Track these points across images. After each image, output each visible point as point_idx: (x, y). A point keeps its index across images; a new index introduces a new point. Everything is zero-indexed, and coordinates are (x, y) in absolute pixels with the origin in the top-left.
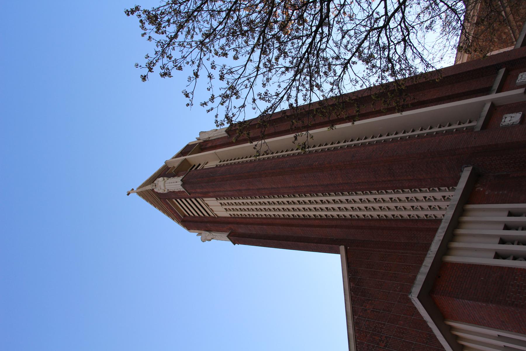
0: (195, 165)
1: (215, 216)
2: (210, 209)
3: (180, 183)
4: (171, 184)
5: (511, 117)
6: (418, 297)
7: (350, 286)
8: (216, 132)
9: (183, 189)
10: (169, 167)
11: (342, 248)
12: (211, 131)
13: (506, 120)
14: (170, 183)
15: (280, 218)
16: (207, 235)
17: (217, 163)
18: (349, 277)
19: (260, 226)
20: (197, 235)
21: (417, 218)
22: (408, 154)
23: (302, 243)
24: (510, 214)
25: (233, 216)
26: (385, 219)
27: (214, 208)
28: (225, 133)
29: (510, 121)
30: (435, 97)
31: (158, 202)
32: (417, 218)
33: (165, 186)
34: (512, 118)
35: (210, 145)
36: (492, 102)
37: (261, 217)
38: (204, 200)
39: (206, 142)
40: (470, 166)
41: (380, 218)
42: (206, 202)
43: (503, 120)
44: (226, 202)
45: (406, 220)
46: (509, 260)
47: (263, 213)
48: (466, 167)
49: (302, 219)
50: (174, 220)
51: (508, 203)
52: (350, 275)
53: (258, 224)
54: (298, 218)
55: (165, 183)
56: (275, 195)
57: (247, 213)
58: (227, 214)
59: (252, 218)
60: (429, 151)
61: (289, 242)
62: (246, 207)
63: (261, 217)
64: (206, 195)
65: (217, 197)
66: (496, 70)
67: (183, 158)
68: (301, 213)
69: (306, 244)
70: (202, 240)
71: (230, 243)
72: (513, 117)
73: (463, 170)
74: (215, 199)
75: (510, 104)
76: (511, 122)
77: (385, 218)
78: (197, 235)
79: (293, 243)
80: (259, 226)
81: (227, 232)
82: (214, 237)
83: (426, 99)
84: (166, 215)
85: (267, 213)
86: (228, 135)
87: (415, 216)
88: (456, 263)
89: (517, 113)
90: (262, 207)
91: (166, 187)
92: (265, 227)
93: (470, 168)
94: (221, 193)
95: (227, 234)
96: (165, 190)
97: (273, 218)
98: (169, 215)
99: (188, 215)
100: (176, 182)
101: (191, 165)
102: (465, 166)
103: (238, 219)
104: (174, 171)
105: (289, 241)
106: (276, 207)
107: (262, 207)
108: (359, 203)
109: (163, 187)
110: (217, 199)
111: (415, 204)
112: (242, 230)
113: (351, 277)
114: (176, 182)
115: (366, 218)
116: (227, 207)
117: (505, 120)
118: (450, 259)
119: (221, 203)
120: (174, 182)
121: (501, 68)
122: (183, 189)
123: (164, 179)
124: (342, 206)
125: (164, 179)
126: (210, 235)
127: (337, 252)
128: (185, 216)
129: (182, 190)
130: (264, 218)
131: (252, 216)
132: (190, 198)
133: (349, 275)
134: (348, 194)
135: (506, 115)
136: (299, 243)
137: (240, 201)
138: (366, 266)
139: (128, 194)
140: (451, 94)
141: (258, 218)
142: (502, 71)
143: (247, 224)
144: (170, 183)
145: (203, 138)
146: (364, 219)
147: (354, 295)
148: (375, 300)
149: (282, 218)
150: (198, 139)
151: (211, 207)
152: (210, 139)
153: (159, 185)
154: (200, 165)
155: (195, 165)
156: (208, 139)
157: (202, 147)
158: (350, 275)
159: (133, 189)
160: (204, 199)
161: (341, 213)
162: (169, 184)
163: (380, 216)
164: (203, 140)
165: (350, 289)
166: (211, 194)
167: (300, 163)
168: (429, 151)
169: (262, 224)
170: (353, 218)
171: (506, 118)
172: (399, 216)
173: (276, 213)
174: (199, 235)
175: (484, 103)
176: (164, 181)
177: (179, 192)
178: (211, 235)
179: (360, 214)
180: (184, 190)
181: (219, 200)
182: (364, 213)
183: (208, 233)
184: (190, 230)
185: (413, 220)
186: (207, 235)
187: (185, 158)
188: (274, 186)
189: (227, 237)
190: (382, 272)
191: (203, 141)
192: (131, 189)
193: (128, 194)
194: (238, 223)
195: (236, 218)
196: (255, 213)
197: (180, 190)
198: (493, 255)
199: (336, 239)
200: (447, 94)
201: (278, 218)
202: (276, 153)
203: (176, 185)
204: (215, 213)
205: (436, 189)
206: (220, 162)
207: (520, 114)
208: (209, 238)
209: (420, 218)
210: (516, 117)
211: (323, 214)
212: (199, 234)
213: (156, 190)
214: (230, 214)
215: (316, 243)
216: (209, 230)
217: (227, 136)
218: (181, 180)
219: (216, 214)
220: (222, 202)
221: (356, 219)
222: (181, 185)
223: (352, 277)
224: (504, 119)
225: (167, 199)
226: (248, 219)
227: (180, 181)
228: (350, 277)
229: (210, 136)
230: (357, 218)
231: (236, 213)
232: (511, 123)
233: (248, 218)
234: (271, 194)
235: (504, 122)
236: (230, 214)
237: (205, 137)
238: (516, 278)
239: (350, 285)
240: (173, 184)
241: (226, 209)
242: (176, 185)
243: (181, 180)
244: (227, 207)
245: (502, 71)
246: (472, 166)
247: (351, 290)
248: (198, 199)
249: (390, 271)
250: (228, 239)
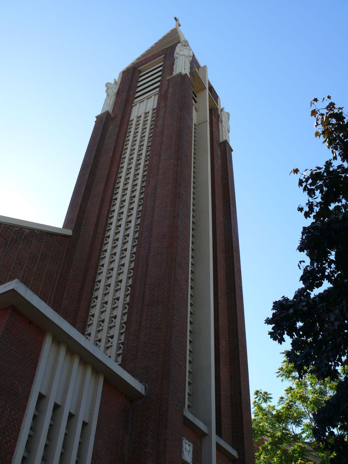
0: (196, 96)
1: (134, 103)
2: (144, 100)
3: (183, 72)
4: (184, 62)
5: (189, 452)
6: (13, 290)
7: (26, 229)
8: (226, 131)
9: (175, 74)
10: (199, 69)
11: (69, 232)
12: (229, 126)
13: (187, 446)
14: (185, 61)
15: (117, 173)
16: (113, 90)
17: (195, 121)
18: (36, 230)
19: (112, 150)
20: (115, 80)
21: (88, 323)
22: (173, 326)
23: (83, 190)
24: (85, 424)
25: (130, 123)
26: (94, 287)
27: (143, 104)
28: (224, 140)
29: (186, 449)
30: (221, 375)
31: (162, 46)
32: (88, 323)
33: (183, 55)
34: (187, 452)
35: (214, 120)
36: (207, 434)
37: (123, 153)
38: (155, 95)
39: (218, 117)
40: (145, 392)
41: (96, 282)
42: (153, 97)
43: (187, 442)
44: (149, 118)
45: (88, 311)
46: (35, 410)
47: (127, 155)
48: (146, 388)
49: (112, 197)
50: (137, 59)
51: (97, 425)
52: (37, 232)
53: (115, 148)
54: (114, 192)
55: (186, 56)
56: (147, 172)
57: (131, 138)
58: (134, 116)
59: (124, 142)
60: (172, 351)
61: (88, 176)
62: (138, 138)
63: (123, 153)
64: (162, 98)
65: (157, 111)
66: (237, 448)
67: (207, 87)
68: (119, 196)
69: (83, 194)
70: (106, 84)
71: (99, 112)
72: (188, 454)
73: (143, 384)
74: (155, 107)
75: (201, 454)
76: (185, 450)
77: (95, 288)
78: (115, 80)
79: (86, 180)
80: (113, 148)
81: (112, 112)
82: (110, 97)
83: (221, 365)
84: (162, 38)
85: (126, 160)
86: (221, 143)
87: (91, 322)
88: (42, 347)
89: (192, 458)
90: (135, 156)
91: (181, 57)
92: (111, 154)
93: (143, 392)
94: (161, 114)
95: (111, 112)
96: (178, 54)
97: (119, 165)
98: (143, 56)
99: (140, 75)
100: (185, 69)
101: (197, 93)
102: (147, 388)
103: (126, 127)
104: (196, 71)
105: (89, 176)
106: (132, 171)
107: (135, 156)
108: (119, 262)
109: (181, 53)
110: (154, 110)
111: (106, 325)
112: (112, 129)
113: (36, 232)
114: (185, 69)
115: (99, 266)
116: (142, 119)
117: (187, 444)
118: (48, 343)
119: (148, 113)
120: (185, 66)
121: (238, 454)
122: (175, 74)
123: (190, 57)
124: (119, 243)
125: (190, 57)
126: (113, 93)
127: (66, 225)
128: (140, 72)
129: (174, 72)
130: (121, 156)
131: (126, 144)
132: (161, 80)
133: (38, 231)
134: (133, 252)
135: (191, 446)
136: (84, 187)
137: (147, 134)
138: (45, 253)
139: (175, 18)
140: (222, 393)
141: (123, 149)
142: (234, 453)
143: (118, 136)
144: (185, 61)
145: (222, 115)
146: (98, 265)
147: (15, 230)
148: (4, 252)
149: (117, 175)
150: (222, 110)
151: (145, 101)
152: (220, 122)
153: (184, 49)
154: (196, 102)
155: (196, 96)
156: (220, 120)
157: (213, 111)
158: (37, 232)
159: (180, 25)
160: (157, 96)
161: (110, 240)
162: (184, 60)
163: (98, 283)
164: (220, 114)
165: (23, 228)
166: (163, 104)
167: (182, 206)
168: (172, 351)
169: (114, 152)
170: (102, 253)
171: (190, 446)
172: (94, 304)
173: (124, 170)
174: (115, 81)
175: (208, 425)
176: (188, 56)
177: (172, 70)
178: (113, 95)
179: (106, 262)
180: (174, 75)
181: (152, 112)
182: (106, 266)
183: (116, 91)
184: (122, 73)
185: (87, 318)
186: (113, 90)
187: (206, 88)
188: (160, 172)
189: (107, 110)
190: (34, 269)
191: (219, 114)
192: (181, 24)
193: (175, 18)
194: (120, 126)
195: (128, 126)
196: (129, 147)
197: (174, 70)
198: (44, 393)
199: (81, 229)
200: (222, 389)
201: (118, 171)
202: (193, 187)
203: (182, 68)
204: (138, 105)
205: (120, 351)
206: (195, 125)
207: (191, 462)
208: (110, 90)
209: (87, 326)
210: (188, 456)
211: (114, 220)
212: (116, 83)
213: (179, 45)
214: (133, 120)
215: (81, 205)
216: (118, 94)
217: (220, 141)
218: (186, 74)
219: (136, 105)
220: (150, 115)
221: (100, 255)
222: (181, 73)
223: (35, 234)
224: (189, 444)
225: (165, 56)
226: (123, 138)
227: (186, 73)
228: (36, 231)
229: (223, 123)
230: (102, 257)
231: (133, 126)
232: (183, 450)
233: (125, 138)
234: (149, 168)
235: (186, 443)
236: (133, 120)
237: (224, 118)
238: (13, 412)
239: (27, 229)
240: (183, 65)
241: (140, 117)
242: (182, 68)
243: (186, 74)
244: (142, 119)
245: (234, 453)
246: (145, 394)
247: (21, 228)
248: (158, 89)
249: (34, 279)
250: (104, 111)
